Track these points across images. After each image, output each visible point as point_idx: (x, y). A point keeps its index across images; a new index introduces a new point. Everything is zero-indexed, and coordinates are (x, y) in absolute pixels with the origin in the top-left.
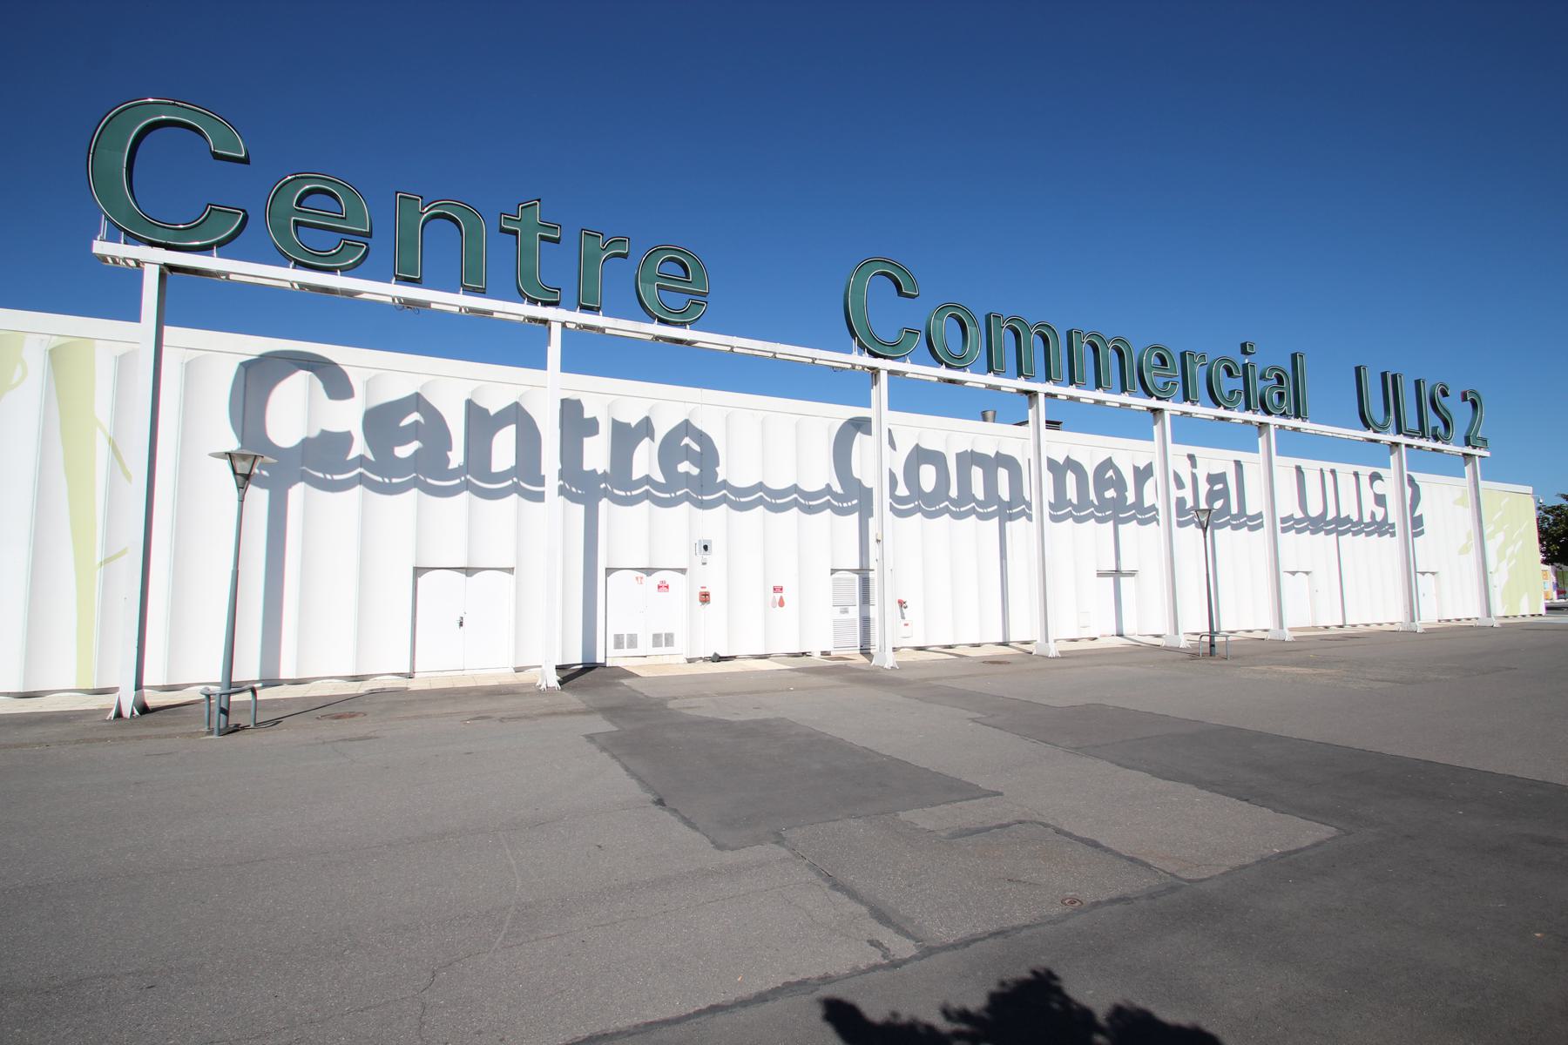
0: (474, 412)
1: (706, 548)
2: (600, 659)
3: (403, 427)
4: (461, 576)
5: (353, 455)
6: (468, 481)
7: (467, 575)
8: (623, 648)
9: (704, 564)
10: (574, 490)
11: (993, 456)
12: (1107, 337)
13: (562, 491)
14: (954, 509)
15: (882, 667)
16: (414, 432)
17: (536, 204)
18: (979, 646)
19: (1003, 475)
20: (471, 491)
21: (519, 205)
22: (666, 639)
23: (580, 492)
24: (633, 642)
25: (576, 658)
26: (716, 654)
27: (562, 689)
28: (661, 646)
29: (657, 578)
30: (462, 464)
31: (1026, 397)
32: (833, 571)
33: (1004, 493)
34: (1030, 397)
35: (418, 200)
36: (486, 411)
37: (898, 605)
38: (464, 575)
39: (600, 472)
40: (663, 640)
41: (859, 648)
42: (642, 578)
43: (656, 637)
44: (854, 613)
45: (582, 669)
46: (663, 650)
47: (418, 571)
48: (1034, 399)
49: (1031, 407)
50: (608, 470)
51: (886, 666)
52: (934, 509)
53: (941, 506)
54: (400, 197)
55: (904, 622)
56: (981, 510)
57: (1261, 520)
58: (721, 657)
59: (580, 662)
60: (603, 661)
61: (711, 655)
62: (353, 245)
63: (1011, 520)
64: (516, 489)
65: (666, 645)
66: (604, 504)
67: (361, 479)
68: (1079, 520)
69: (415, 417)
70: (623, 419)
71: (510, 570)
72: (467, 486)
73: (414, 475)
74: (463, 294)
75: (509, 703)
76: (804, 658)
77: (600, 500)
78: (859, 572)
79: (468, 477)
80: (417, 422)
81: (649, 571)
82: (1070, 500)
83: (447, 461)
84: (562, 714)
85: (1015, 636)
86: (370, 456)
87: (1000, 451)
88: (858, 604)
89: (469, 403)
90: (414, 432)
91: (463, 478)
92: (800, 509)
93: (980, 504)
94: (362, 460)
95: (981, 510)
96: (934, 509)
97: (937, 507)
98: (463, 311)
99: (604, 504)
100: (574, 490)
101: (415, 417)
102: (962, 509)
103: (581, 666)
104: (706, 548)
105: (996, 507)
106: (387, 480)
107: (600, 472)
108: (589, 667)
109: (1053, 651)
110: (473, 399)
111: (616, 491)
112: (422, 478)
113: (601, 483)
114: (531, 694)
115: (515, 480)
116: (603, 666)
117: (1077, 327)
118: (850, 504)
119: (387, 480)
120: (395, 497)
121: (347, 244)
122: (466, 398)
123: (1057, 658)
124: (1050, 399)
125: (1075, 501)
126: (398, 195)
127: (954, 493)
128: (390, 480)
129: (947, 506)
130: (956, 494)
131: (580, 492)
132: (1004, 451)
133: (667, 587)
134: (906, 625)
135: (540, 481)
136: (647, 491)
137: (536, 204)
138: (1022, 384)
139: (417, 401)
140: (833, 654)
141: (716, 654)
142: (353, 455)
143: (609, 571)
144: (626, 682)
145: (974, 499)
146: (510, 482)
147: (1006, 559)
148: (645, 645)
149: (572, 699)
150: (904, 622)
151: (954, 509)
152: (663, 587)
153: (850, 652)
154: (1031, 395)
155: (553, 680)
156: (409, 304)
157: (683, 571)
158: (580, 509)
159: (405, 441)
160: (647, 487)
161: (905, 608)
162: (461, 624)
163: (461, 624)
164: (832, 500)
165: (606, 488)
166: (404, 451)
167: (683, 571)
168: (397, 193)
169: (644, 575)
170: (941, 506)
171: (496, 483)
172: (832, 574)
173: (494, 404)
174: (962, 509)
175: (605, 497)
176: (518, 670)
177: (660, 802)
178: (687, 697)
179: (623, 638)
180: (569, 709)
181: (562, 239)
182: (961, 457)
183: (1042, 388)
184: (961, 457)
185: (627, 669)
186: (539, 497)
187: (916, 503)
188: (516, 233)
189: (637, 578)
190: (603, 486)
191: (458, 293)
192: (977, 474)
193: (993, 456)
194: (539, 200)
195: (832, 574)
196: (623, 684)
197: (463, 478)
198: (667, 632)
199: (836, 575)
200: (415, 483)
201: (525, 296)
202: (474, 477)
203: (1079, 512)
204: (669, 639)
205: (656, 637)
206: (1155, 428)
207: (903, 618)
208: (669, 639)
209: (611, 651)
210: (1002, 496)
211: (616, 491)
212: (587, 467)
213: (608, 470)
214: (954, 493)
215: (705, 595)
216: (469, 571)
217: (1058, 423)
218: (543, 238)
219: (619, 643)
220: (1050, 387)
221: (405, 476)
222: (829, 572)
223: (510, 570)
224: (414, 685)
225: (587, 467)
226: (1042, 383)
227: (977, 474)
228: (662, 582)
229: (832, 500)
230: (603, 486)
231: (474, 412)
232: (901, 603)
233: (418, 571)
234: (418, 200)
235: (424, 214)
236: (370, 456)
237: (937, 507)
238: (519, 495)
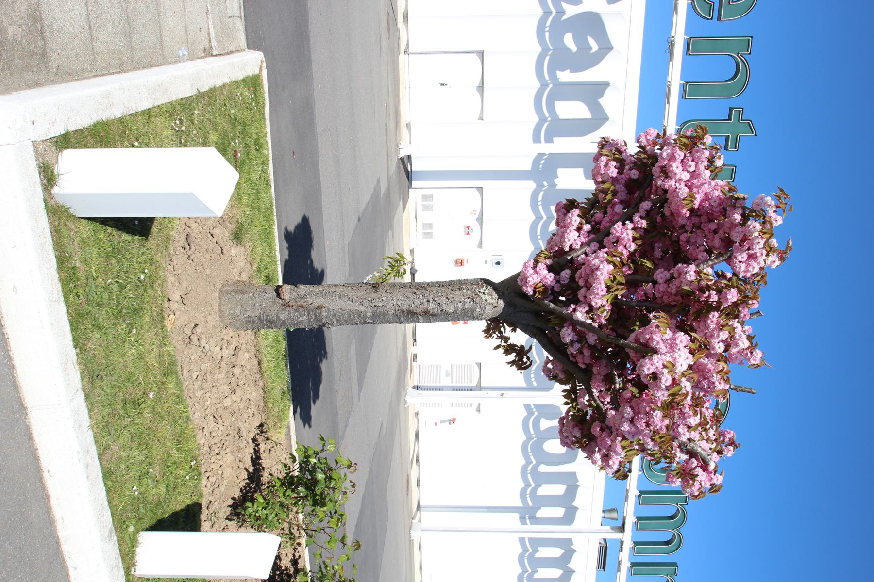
0: (601, 88)
1: (498, 263)
2: (415, 184)
3: (587, 39)
4: (477, 83)
5: (565, 5)
6: (547, 85)
7: (478, 87)
8: (423, 201)
9: (486, 262)
10: (543, 162)
11: (574, 504)
12: (683, 529)
13: (540, 156)
14: (530, 468)
15: (406, 394)
16: (584, 47)
17: (753, 133)
18: (418, 485)
19: (558, 512)
20: (540, 88)
21: (751, 121)
22: (428, 233)
23: (541, 166)
24: (426, 208)
25: (416, 166)
26: (416, 271)
27: (398, 159)
28: (423, 229)
29: (476, 226)
30: (560, 80)
31: (620, 524)
32: (479, 365)
33: (542, 513)
34: (620, 528)
35: (748, 52)
36: (601, 96)
37: (451, 418)
38: (478, 85)
39: (556, 181)
40: (428, 231)
41: (419, 385)
42: (475, 214)
43: (430, 226)
44: (446, 382)
45: (408, 170)
46: (421, 231)
47: (481, 54)
48: (618, 530)
49: (612, 528)
50: (558, 187)
51: (407, 397)
52: (529, 451)
53: (532, 458)
54: (749, 40)
55: (438, 423)
56: (528, 492)
57: (533, 407)
58: (414, 275)
59: (413, 170)
60: (413, 186)
61: (415, 268)
62: (710, 10)
63: (520, 518)
64: (543, 120)
65: (424, 234)
66: (531, 185)
67: (547, 13)
68: (521, 558)
69: (595, 47)
70: (608, 93)
71: (481, 118)
72: (544, 85)
73: (551, 48)
74: (680, 84)
75: (392, 124)
76: (412, 341)
77: (535, 182)
78: (479, 386)
79: (551, 86)
80: (591, 48)
81: (480, 220)
82: (537, 571)
83: (563, 70)
84: (388, 162)
85: (424, 514)
86: (565, 17)
87: (578, 511)
88: (453, 385)
89: (606, 85)
90: (584, 47)
91: (549, 82)
92: (524, 465)
93: (536, 467)
94: (561, 12)
95: (528, 492)
96: (529, 451)
97: (531, 454)
98: (669, 83)
99: (531, 185)
100: (543, 162)
101: (595, 47)
102: (529, 476)
103: (409, 170)
104: (498, 263)
105: (531, 504)
106: (539, 237)
107: (556, 181)
108: (409, 176)
109: (415, 535)
110: (610, 87)
111: (542, 193)
112: (550, 53)
113: (547, 182)
114: (396, 139)
115: (549, 119)
116: (410, 186)
117: (680, 570)
118: (533, 379)
119: (547, 29)
120: (534, 73)
121: (711, 6)
122: (610, 82)
123: (410, 537)
124: (619, 544)
125: (537, 555)
126: (750, 38)
127: (543, 468)
128: (547, 31)
129: (532, 462)
130: (542, 471)
131: (541, 166)
132: (578, 513)
133: (468, 234)
134: (436, 424)
135: (549, 140)
136: (542, 218)
137: (753, 133)
138: (630, 521)
139: (606, 48)
140: (414, 364)
141: (416, 271)
142: (565, 5)
143: (480, 190)
144: (401, 203)
145: (538, 486)
146: (547, 115)
147: (488, 512)
148: (425, 217)
149: (394, 164)
150: (438, 423)
151: (530, 468)
152: (468, 230)
153: (415, 378)
154: (622, 529)
155: (403, 153)
156: (671, 46)
157: (480, 246)
158: (527, 166)
159: (576, 40)
160: (545, 217)
161: (450, 424)
162: (442, 85)
163: (442, 85)
164: (532, 465)
165: (544, 186)
166: (569, 40)
167: (480, 246)
168: (752, 37)
169: (477, 216)
170: (532, 458)
171: (547, 127)
172: (477, 364)
173: (606, 101)
174: (529, 476)
175: (537, 186)
176: (408, 126)
177: (359, 220)
178: (394, 244)
179: (430, 201)
180: (390, 166)
181: (728, 152)
182: (573, 475)
183: (628, 537)
184: (573, 475)
185: (408, 204)
186: (536, 139)
187: (534, 436)
188: (730, 119)
189: (475, 211)
190: (545, 183)
191: (681, 79)
192: (559, 489)
193: (574, 504)
194: (756, 135)
195: (477, 364)
196: (400, 201)
197: (549, 82)
198: (433, 234)
199: (476, 368)
200: (545, 50)
201: (682, 126)
202: (554, 17)
203: (527, 559)
204: (428, 235)
205: (430, 226)
206: (608, 528)
207: (441, 422)
208: (428, 235)
209: (420, 193)
210: (540, 510)
211: (542, 193)
212: (560, 171)
213: (558, 187)
214: (543, 468)
215: (461, 263)
216: (481, 88)
217: (604, 568)
218: (727, 138)
219: (426, 198)
220: (628, 545)
221: (550, 43)
222: (479, 362)
223: (481, 118)
224: (402, 58)
225: (560, 171)
226: (632, 537)
227: (559, 489)
228: (472, 230)
229: (532, 465)
230: (545, 183)
231: (601, 88)
232: (454, 420)
233: (481, 54)
234: (748, 52)
235: (738, 56)
236: (565, 17)
237: (531, 454)
238: (538, 122)
